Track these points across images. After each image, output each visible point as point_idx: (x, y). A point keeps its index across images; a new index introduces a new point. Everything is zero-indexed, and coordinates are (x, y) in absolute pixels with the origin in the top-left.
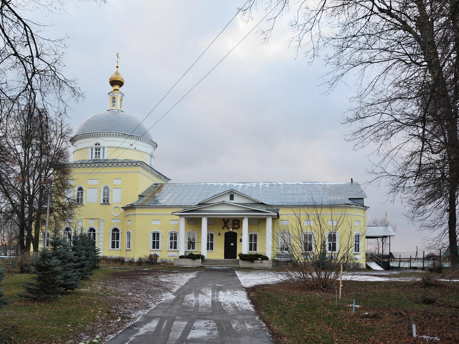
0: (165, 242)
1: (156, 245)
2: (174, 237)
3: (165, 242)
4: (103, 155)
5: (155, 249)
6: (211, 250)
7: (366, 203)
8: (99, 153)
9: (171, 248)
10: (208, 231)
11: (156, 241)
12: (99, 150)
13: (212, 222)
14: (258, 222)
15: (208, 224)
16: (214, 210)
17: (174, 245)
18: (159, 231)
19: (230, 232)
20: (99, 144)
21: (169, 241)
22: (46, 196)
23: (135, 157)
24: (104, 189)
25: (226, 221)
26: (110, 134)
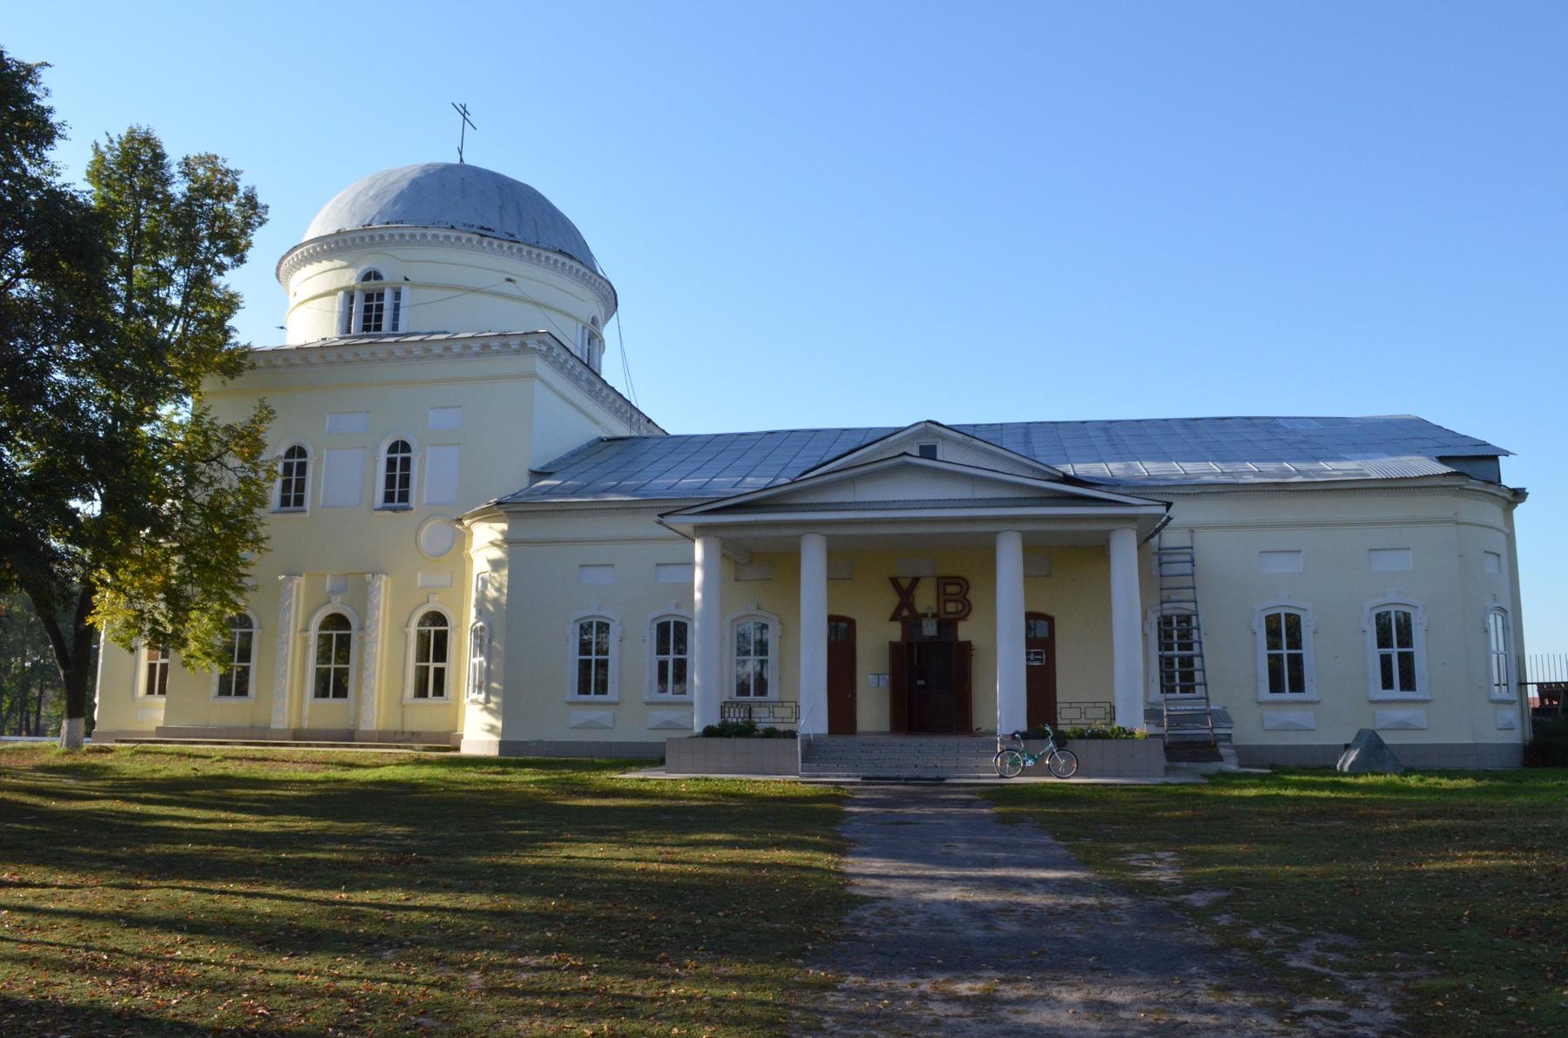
0: (632, 659)
1: (592, 676)
2: (671, 635)
3: (632, 659)
4: (396, 317)
5: (592, 697)
6: (1292, 690)
7: (1510, 476)
8: (380, 308)
9: (1387, 683)
10: (831, 598)
11: (593, 657)
12: (381, 296)
13: (846, 560)
14: (1070, 556)
15: (831, 579)
16: (859, 499)
17: (674, 674)
18: (609, 614)
19: (449, 1013)
20: (377, 276)
21: (650, 659)
22: (201, 496)
23: (518, 320)
24: (393, 448)
25: (905, 584)
26: (424, 236)
